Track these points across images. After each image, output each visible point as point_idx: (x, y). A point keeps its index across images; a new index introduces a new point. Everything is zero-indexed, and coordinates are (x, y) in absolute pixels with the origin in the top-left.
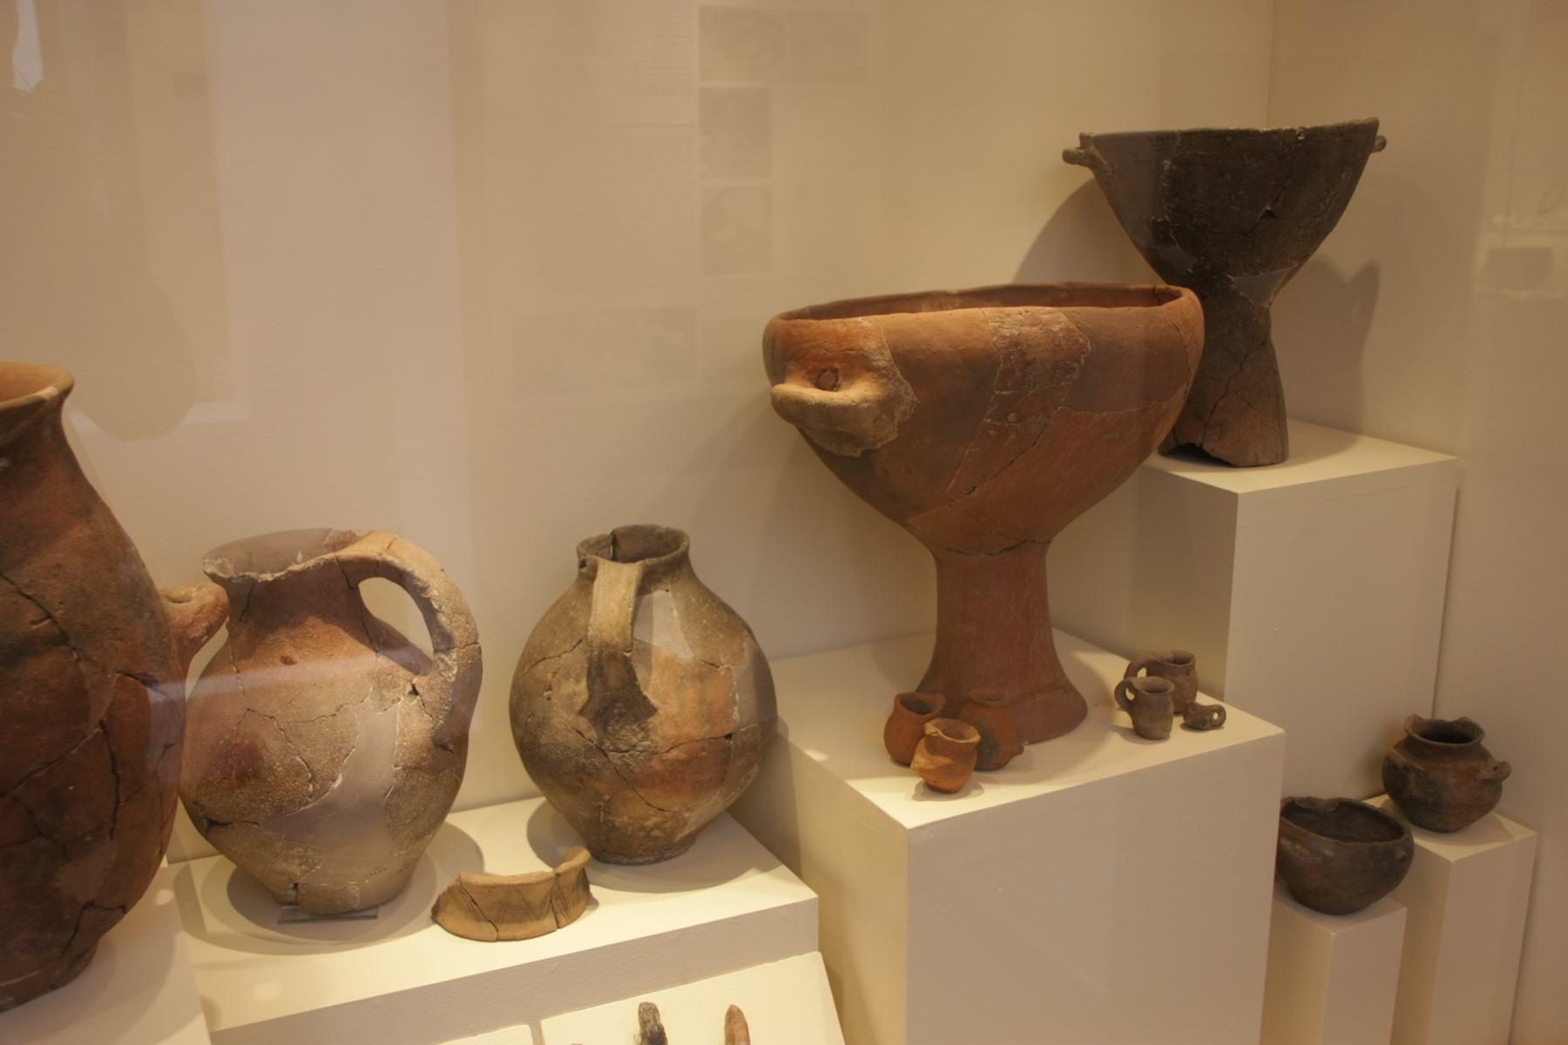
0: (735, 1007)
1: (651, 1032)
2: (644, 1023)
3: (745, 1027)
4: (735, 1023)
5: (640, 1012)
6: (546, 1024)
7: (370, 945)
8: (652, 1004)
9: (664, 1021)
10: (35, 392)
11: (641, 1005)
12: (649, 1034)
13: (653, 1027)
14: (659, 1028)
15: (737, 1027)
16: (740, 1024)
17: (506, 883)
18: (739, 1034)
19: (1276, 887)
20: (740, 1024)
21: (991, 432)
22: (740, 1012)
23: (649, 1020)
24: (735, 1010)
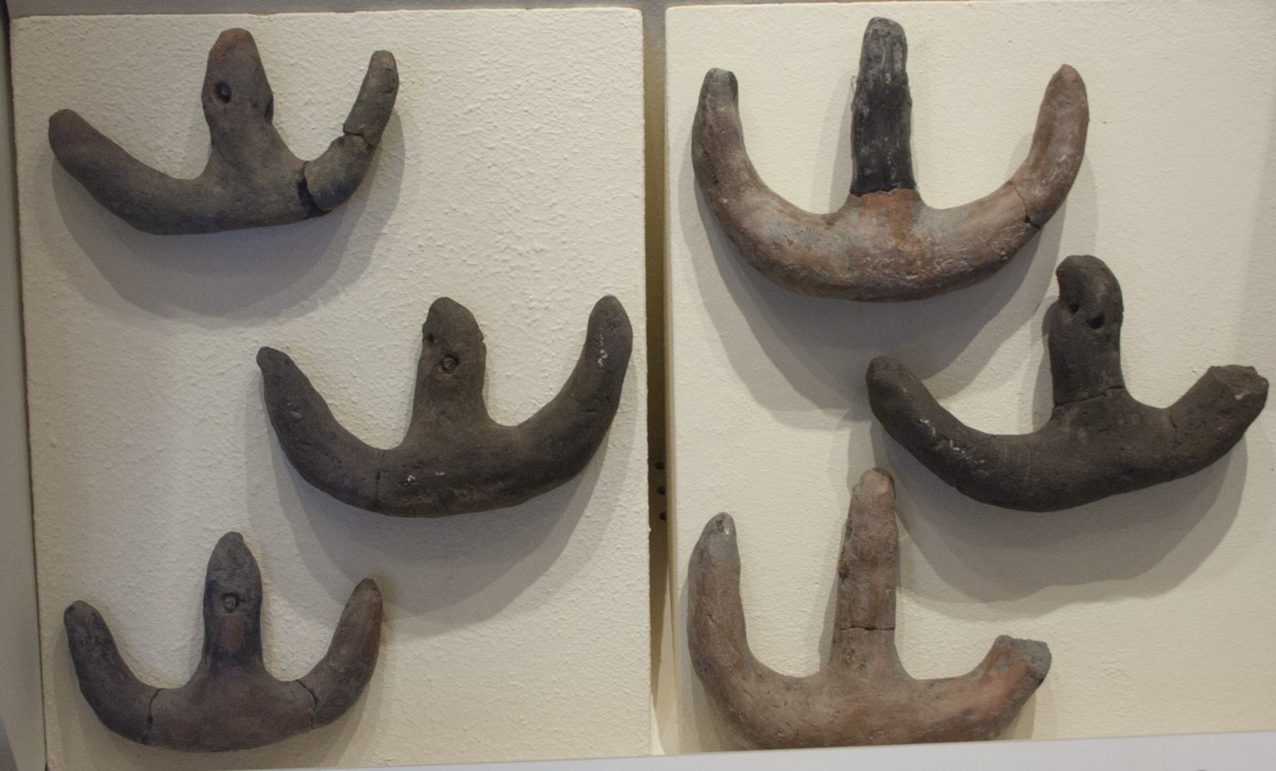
0: (1073, 71)
1: (876, 81)
2: (868, 60)
3: (1083, 118)
4: (1061, 104)
5: (866, 36)
6: (674, 14)
7: (672, 319)
8: (896, 26)
9: (914, 69)
10: (1054, 264)
11: (872, 22)
12: (871, 85)
13: (883, 72)
14: (894, 78)
15: (1062, 113)
16: (1069, 110)
17: (666, 187)
18: (1066, 129)
19: (1004, 738)
20: (1069, 110)
21: (534, 81)
22: (1078, 83)
23: (878, 58)
24: (1068, 77)
